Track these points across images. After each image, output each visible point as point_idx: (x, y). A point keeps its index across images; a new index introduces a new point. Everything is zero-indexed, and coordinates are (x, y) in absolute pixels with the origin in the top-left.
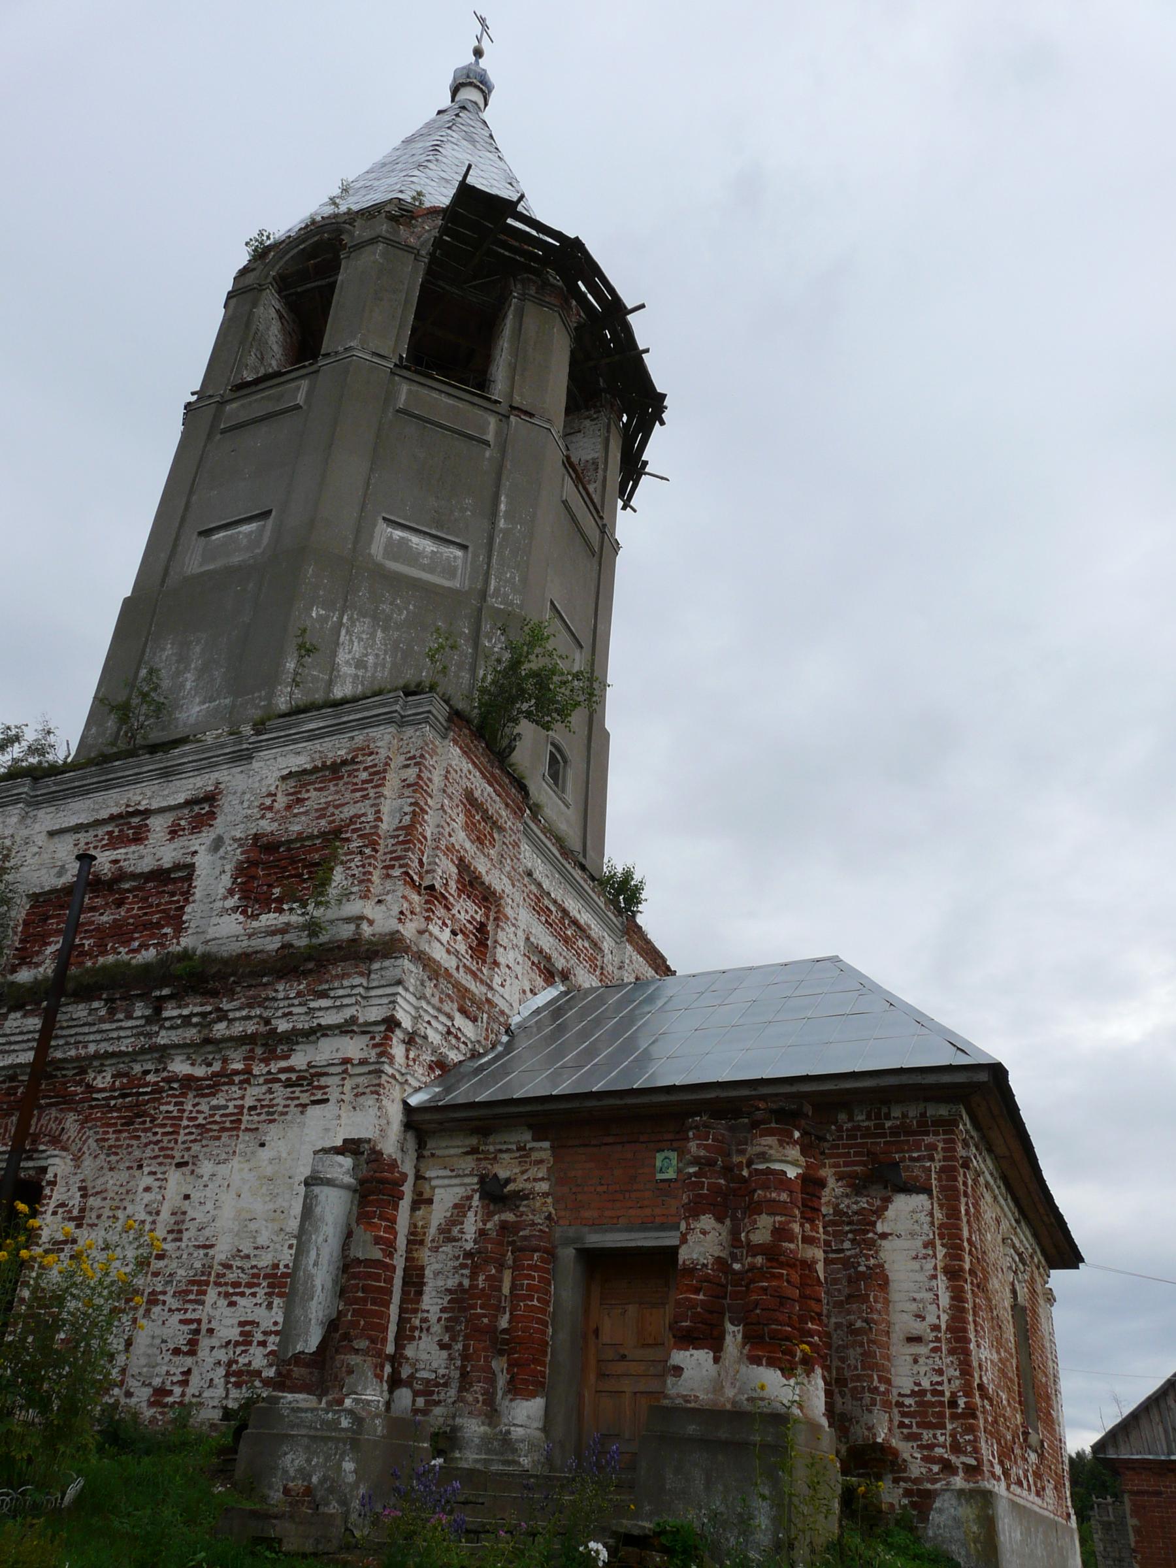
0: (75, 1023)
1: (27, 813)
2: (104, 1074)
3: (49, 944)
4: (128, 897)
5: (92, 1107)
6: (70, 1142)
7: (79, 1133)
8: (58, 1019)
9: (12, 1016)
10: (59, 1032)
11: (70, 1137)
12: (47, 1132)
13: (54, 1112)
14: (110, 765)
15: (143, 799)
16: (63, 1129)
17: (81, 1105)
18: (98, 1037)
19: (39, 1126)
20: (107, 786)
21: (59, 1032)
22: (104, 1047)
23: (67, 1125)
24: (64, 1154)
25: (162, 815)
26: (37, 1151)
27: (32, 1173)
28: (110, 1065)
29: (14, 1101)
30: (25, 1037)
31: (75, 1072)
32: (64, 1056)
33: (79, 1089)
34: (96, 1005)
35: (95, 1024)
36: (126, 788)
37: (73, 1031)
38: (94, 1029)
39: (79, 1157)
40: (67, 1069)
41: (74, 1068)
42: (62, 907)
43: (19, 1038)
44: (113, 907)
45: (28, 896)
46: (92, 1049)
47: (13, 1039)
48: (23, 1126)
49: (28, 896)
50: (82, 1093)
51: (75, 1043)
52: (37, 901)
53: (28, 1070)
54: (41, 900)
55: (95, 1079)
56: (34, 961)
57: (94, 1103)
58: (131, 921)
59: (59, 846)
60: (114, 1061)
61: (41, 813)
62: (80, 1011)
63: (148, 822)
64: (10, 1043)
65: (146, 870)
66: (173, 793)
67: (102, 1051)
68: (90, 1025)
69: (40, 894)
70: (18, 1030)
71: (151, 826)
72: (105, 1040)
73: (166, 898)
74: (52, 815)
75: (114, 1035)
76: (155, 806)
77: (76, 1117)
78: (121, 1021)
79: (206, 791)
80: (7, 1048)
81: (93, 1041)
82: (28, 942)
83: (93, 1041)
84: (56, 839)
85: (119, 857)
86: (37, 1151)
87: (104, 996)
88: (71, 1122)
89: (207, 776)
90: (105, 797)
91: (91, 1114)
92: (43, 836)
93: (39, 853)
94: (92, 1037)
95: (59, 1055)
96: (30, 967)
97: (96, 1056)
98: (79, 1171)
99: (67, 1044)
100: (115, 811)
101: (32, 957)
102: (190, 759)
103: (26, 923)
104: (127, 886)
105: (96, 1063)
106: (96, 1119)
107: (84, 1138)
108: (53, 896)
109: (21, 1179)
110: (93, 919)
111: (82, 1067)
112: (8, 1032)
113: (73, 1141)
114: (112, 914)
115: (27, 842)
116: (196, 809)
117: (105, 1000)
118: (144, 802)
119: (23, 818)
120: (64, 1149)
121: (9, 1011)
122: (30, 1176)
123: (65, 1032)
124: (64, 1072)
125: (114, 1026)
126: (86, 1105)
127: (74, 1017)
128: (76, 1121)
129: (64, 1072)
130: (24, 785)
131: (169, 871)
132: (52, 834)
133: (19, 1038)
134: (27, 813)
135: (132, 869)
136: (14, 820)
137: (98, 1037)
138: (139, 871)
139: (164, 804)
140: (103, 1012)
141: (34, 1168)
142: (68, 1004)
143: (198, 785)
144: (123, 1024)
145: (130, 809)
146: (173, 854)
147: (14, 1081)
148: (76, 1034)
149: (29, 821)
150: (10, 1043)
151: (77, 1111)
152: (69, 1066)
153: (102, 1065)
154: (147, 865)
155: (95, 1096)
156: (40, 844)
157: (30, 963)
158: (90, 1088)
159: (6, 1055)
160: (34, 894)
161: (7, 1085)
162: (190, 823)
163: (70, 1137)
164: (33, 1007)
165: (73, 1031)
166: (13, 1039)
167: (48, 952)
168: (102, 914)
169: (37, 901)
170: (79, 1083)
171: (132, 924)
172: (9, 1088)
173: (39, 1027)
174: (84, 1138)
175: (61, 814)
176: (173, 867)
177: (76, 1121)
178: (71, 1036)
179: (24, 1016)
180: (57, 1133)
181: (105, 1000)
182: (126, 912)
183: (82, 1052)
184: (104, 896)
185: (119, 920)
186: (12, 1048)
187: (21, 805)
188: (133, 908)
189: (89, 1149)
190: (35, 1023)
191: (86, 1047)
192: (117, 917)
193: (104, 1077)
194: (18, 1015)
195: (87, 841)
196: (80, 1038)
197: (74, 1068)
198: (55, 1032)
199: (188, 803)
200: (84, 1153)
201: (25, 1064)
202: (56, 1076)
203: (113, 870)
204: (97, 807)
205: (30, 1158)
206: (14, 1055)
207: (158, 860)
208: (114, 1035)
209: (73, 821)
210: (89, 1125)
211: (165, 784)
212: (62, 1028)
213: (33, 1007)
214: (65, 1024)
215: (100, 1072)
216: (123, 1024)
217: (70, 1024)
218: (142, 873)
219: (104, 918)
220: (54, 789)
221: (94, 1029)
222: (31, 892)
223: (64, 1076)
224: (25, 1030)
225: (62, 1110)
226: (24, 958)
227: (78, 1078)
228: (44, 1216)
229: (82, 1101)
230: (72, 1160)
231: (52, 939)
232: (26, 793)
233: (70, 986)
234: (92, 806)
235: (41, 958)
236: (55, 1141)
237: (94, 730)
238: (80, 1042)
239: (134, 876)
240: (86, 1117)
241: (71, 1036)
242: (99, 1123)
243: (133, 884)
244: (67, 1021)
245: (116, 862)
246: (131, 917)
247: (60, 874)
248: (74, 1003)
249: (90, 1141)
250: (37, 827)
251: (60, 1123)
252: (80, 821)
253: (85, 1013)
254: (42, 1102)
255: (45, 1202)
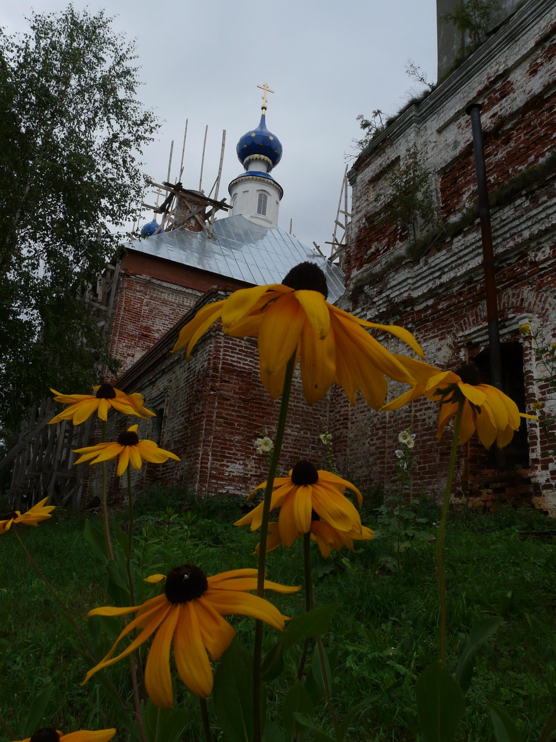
0: (506, 222)
1: (419, 129)
2: (543, 249)
3: (464, 193)
4: (513, 134)
5: (542, 276)
6: (532, 306)
7: (537, 298)
8: (492, 226)
9: (456, 240)
10: (495, 234)
11: (530, 303)
12: (510, 306)
13: (510, 291)
14: (466, 61)
15: (500, 66)
16: (522, 299)
17: (531, 278)
18: (529, 223)
19: (502, 305)
20: (468, 77)
21: (495, 234)
22: (535, 229)
23: (525, 295)
24: (530, 315)
25: (519, 68)
26: (508, 319)
27: (508, 337)
28: (546, 241)
29: (477, 295)
30: (470, 249)
31: (517, 258)
32: (505, 249)
33: (525, 268)
34: (518, 202)
35: (523, 215)
36: (484, 68)
37: (506, 229)
38: (524, 218)
39: (545, 313)
40: (510, 258)
41: (516, 255)
42: (464, 167)
43: (467, 251)
44: (503, 146)
45: (438, 173)
46: (526, 234)
47: (461, 254)
48: (492, 307)
49: (438, 173)
50: (529, 270)
51: (511, 236)
52: (445, 173)
53: (482, 270)
54: (448, 171)
55: (536, 256)
56: (456, 209)
57: (542, 272)
58: (522, 146)
59: (447, 135)
60: (548, 236)
61: (428, 124)
62: (508, 212)
63: (509, 79)
64: (460, 258)
65: (521, 105)
66: (523, 46)
67: (536, 232)
68: (519, 217)
69: (446, 166)
70: (463, 247)
71: (512, 81)
72: (536, 223)
73: (546, 114)
74: (436, 120)
75: (543, 215)
76: (510, 63)
77: (530, 288)
78: (546, 202)
79: (551, 25)
80: (459, 262)
81: (526, 228)
82: (448, 201)
83: (526, 228)
84: (444, 133)
85: (496, 111)
86: (508, 319)
87: (524, 192)
88: (527, 293)
89: (549, 15)
90: (470, 85)
91: (543, 281)
92: (435, 134)
93: (436, 146)
94: (523, 226)
95: (500, 250)
96: (455, 214)
97: (532, 238)
98: (548, 323)
99: (504, 240)
100: (480, 88)
101: (454, 207)
102: (529, 12)
103: (442, 190)
104: (509, 126)
105: (532, 245)
106: (549, 283)
107: (543, 299)
108: (455, 164)
109: (502, 343)
110: (490, 161)
111: (522, 252)
112: (457, 250)
113: (535, 304)
114: (504, 150)
115: (425, 144)
116: (547, 44)
117: (525, 195)
118: (501, 67)
119: (418, 133)
120: (531, 312)
121: (452, 239)
122: (507, 339)
123: (500, 232)
124: (508, 262)
125: (540, 209)
126: (536, 276)
127: (503, 218)
128: (531, 290)
129: (508, 262)
130: (412, 111)
131: (541, 94)
132: (440, 131)
133: (467, 251)
134: (419, 129)
135: (509, 111)
136: (413, 135)
137: (529, 223)
138: (515, 108)
139: (519, 56)
140: (527, 204)
141: (509, 333)
142: (495, 213)
143: (543, 26)
144: (548, 204)
145: (492, 79)
146: (541, 81)
147: (471, 283)
148: (510, 229)
149: (422, 133)
150: (460, 258)
151: (529, 284)
152: (511, 255)
153: (539, 243)
154: (521, 102)
155: (541, 267)
156: (435, 140)
157: (454, 211)
158: (534, 264)
159: (460, 268)
160: (442, 168)
161: (467, 288)
162: (545, 58)
163: (530, 303)
164: (469, 227)
165: (506, 229)
166: (461, 254)
167: (464, 199)
168: (496, 155)
169: (445, 173)
170: (524, 263)
171: (524, 148)
172: (469, 289)
173: (480, 236)
174: (543, 299)
175: (442, 115)
176: (544, 89)
177: (531, 290)
178: (506, 232)
179: (465, 236)
180: (518, 304)
181: (525, 195)
182: (516, 142)
183: (519, 240)
184: (492, 144)
185: (512, 150)
186: (463, 260)
187: (414, 124)
188: (520, 137)
189: (550, 305)
190: (475, 236)
191: (521, 235)
192: (509, 149)
193: (544, 252)
194: (460, 237)
195: (465, 120)
196: (515, 231)
197: (516, 255)
198: (492, 235)
199: (539, 44)
200: (547, 309)
201: (476, 267)
202: (503, 267)
203: (494, 121)
204: (465, 95)
205: (504, 327)
206: (466, 265)
207: (529, 93)
208: (543, 215)
209: (452, 113)
210: (544, 289)
211: (514, 45)
212: (497, 230)
213: (469, 227)
214: (498, 227)
215: (538, 250)
216: (548, 204)
217: (502, 224)
218: (520, 108)
219: (499, 156)
220: (432, 102)
221: (524, 218)
222: (439, 169)
223: (509, 265)
224: (468, 244)
225: (516, 288)
226: (449, 210)
227: (521, 261)
228: (530, 362)
229: (531, 274)
230: (538, 318)
231: (464, 190)
232: (414, 115)
233: (493, 200)
234: (462, 96)
235: (462, 204)
236: (519, 309)
237: (445, 59)
238: (515, 234)
239: (513, 115)
240: (539, 284)
241: (506, 232)
242: (552, 285)
243: (513, 122)
244: (498, 224)
245: (494, 115)
246: (521, 143)
247: (455, 147)
248: (500, 210)
249: (549, 299)
250: (429, 132)
251: (518, 297)
252: (457, 110)
253: (512, 211)
254: (499, 287)
255: (527, 352)
